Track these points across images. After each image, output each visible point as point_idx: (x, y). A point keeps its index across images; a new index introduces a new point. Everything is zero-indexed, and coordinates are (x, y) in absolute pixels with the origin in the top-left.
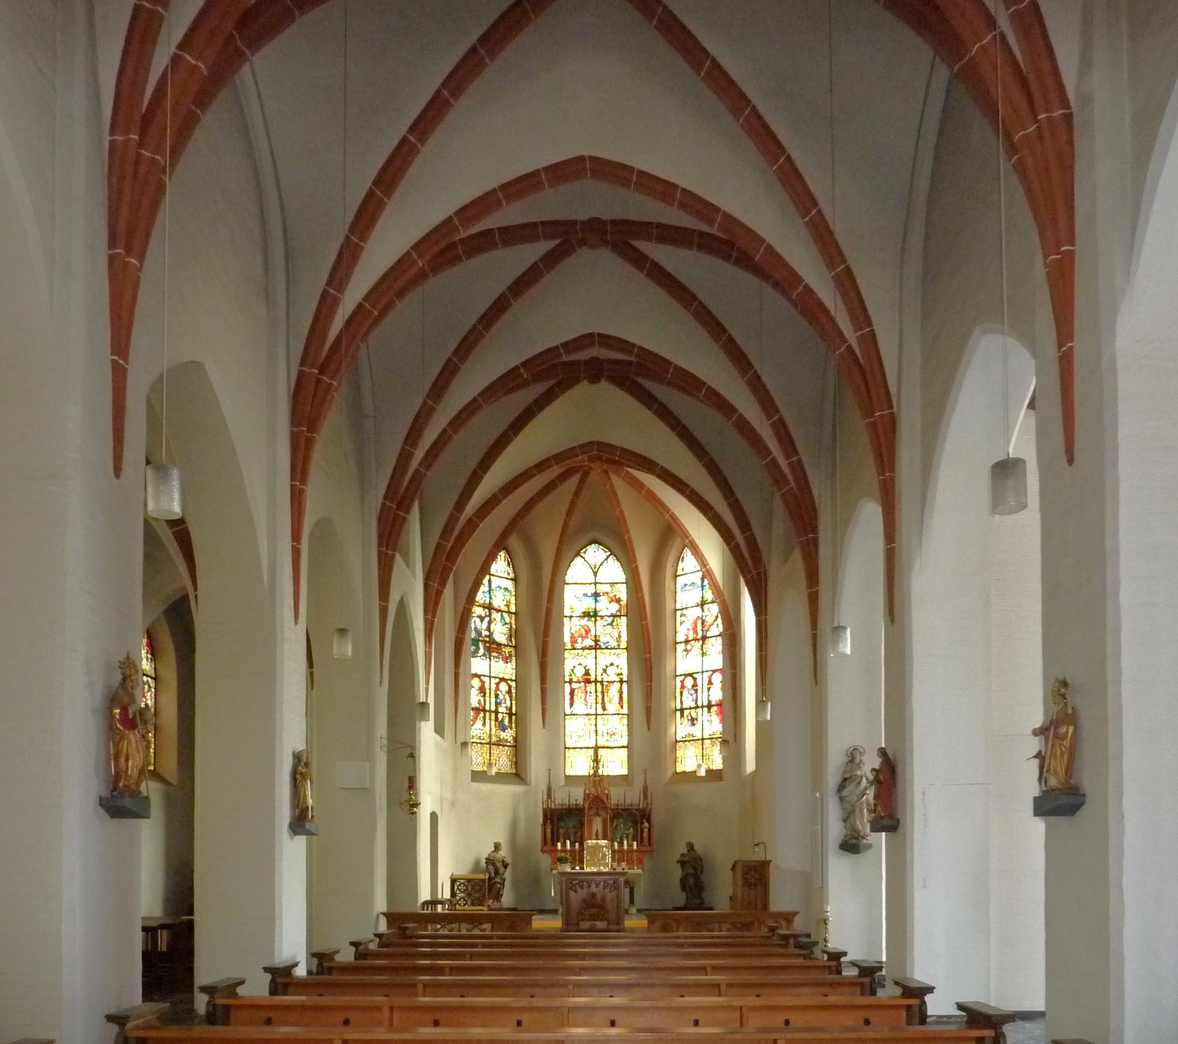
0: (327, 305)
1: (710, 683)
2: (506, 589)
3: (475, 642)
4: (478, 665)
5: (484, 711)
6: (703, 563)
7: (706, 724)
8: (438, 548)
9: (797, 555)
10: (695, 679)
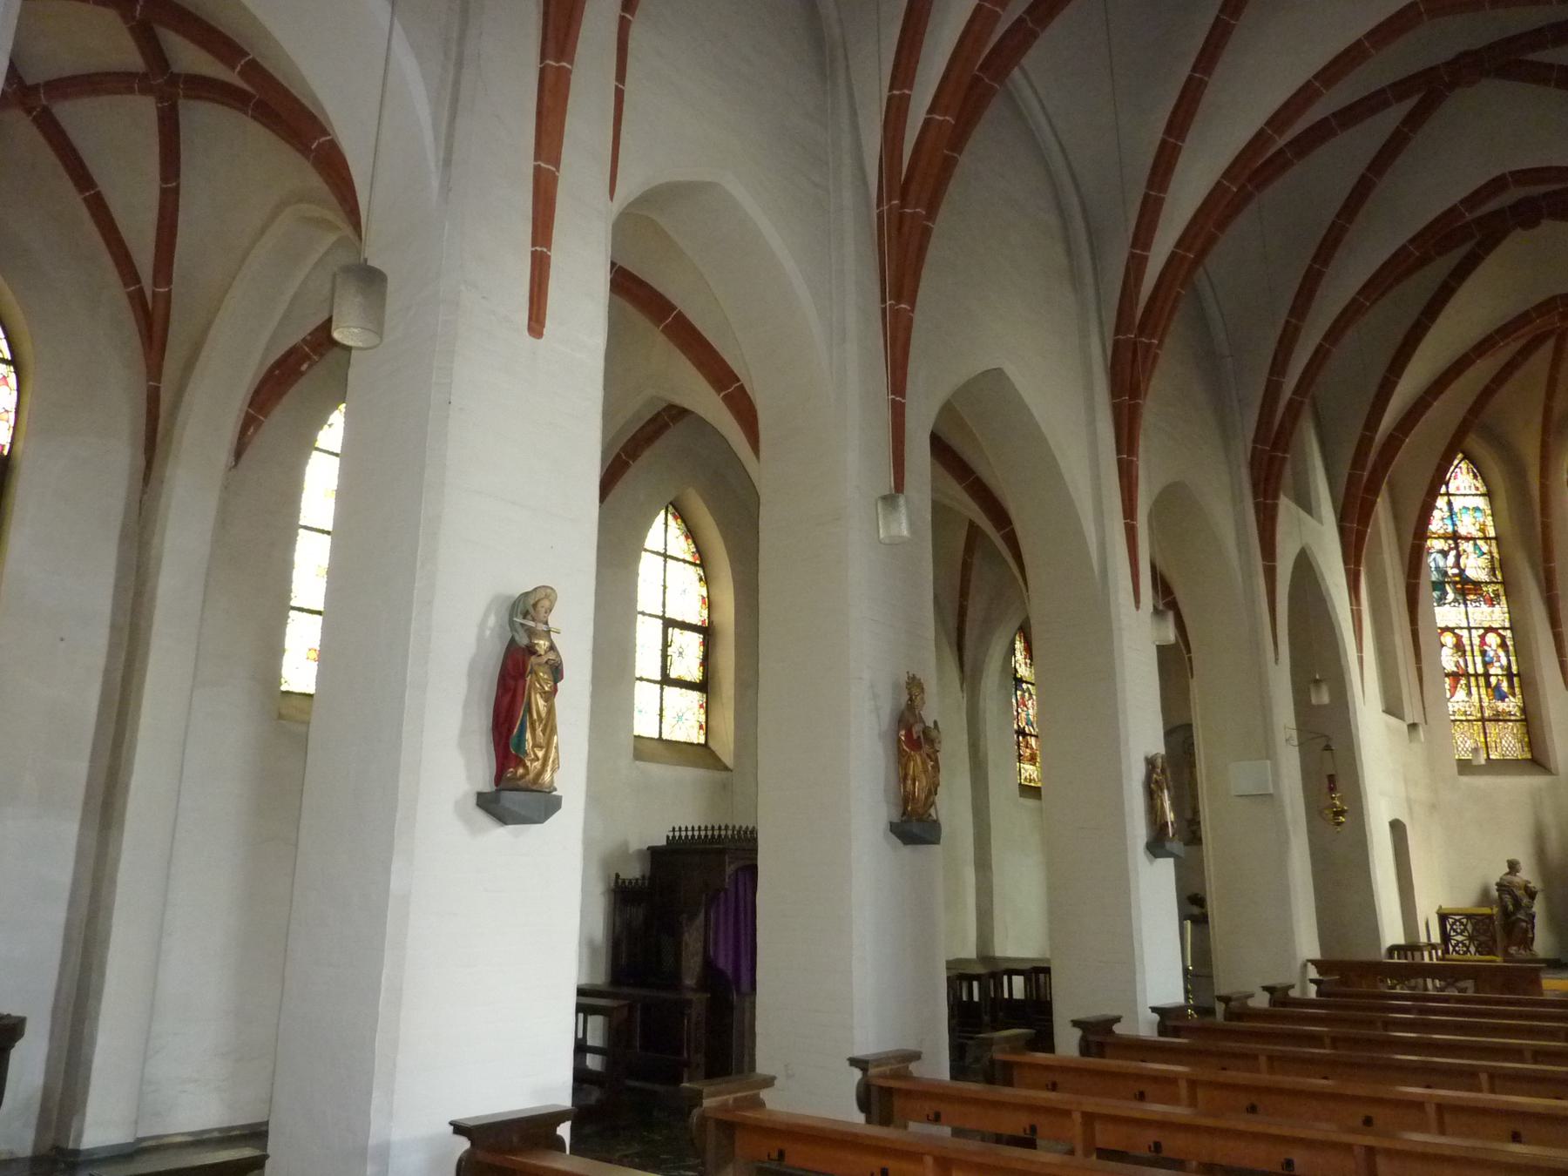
0: (1136, 266)
2: (1477, 509)
3: (1439, 586)
4: (1448, 614)
5: (1468, 676)
8: (1352, 481)
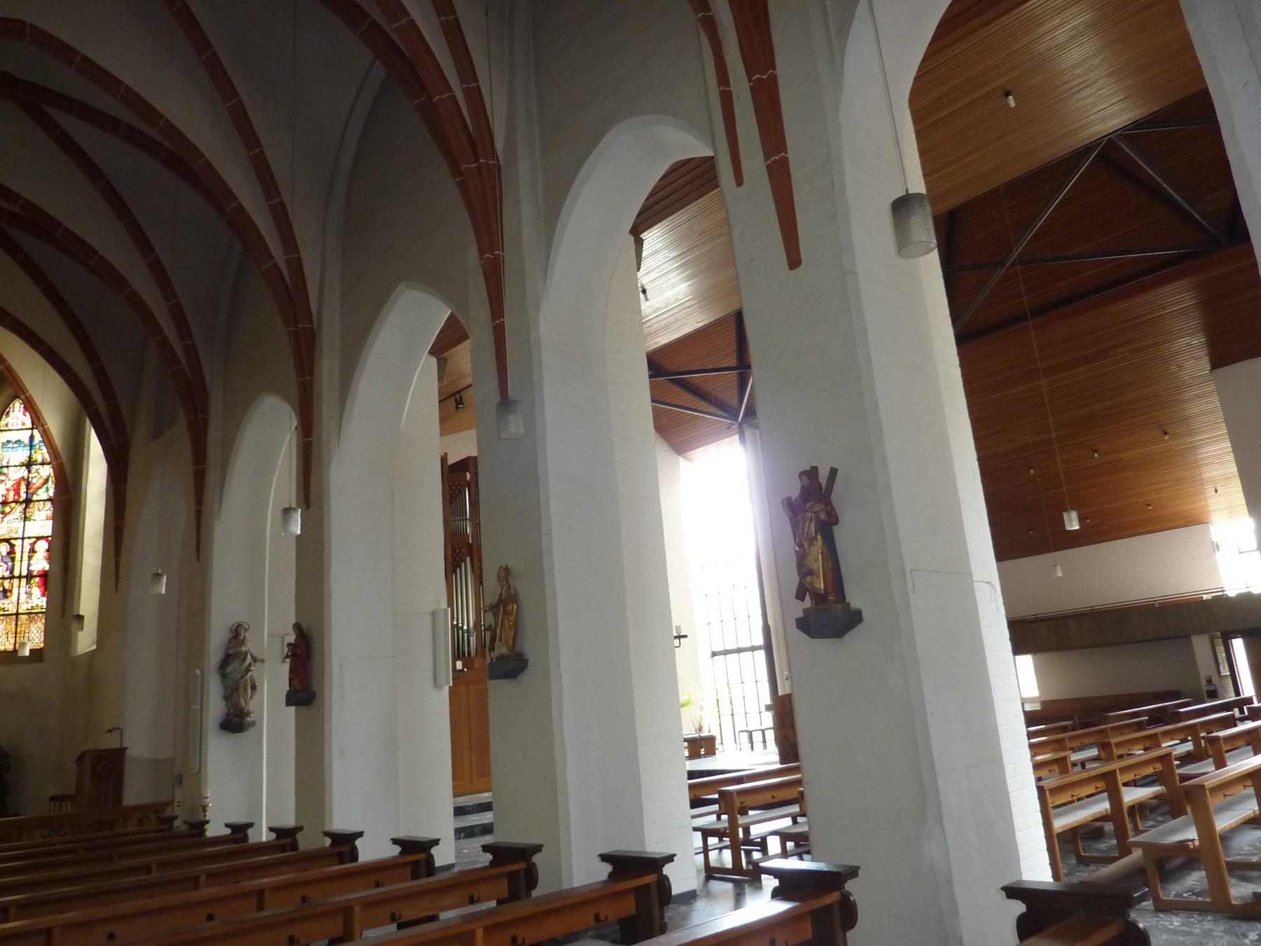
1: (32, 551)
6: (38, 421)
7: (23, 597)
9: (180, 430)
10: (12, 546)
